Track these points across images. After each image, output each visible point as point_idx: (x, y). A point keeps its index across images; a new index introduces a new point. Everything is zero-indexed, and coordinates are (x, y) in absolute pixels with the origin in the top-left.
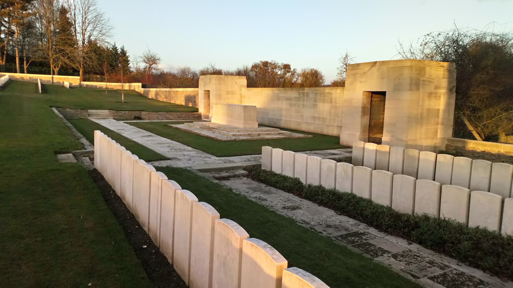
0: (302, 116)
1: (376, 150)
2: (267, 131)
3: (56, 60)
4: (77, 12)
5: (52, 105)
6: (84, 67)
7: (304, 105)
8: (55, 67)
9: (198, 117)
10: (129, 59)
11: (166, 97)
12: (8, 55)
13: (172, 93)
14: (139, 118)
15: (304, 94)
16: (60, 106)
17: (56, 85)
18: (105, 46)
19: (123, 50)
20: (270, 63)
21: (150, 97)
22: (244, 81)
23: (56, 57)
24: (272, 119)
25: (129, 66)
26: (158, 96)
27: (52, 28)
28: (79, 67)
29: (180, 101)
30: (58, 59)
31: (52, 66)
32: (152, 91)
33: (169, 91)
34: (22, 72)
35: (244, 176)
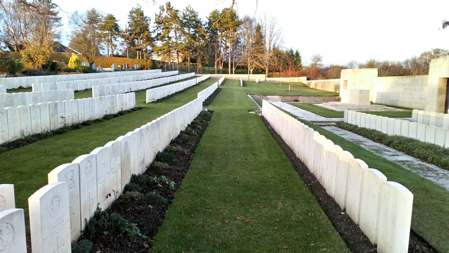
0: (413, 97)
1: (424, 115)
2: (376, 107)
3: (252, 64)
4: (267, 28)
5: (248, 93)
6: (269, 68)
7: (414, 89)
8: (251, 69)
9: (338, 100)
10: (301, 58)
11: (322, 87)
12: (224, 62)
13: (326, 83)
14: (297, 101)
15: (415, 80)
16: (252, 94)
17: (251, 81)
18: (284, 50)
19: (297, 52)
20: (442, 50)
21: (311, 87)
22: (375, 71)
23: (252, 62)
24: (393, 100)
25: (301, 63)
26: (317, 86)
27: (251, 41)
28: (266, 67)
29: (331, 89)
30: (253, 63)
31: (249, 68)
32: (313, 83)
33: (324, 82)
34: (232, 73)
35: (334, 125)
